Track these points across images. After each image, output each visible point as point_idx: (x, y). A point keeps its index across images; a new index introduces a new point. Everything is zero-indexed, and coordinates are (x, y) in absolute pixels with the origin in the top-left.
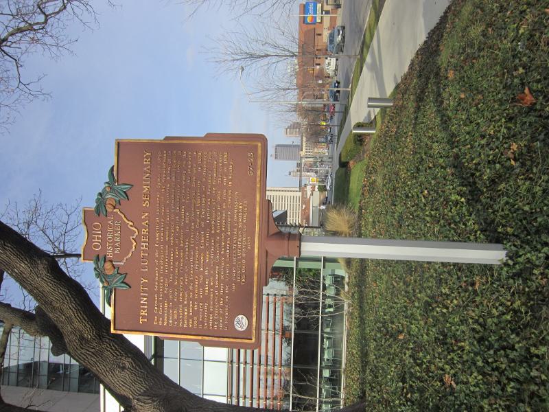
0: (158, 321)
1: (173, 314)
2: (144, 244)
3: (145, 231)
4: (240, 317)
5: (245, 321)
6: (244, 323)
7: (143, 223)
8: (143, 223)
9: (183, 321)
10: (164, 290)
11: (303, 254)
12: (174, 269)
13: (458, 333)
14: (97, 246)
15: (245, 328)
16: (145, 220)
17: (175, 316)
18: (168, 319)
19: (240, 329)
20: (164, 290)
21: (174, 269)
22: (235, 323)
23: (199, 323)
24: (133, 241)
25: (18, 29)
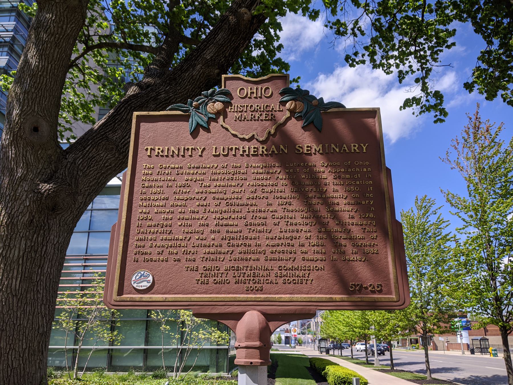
22: (142, 273)
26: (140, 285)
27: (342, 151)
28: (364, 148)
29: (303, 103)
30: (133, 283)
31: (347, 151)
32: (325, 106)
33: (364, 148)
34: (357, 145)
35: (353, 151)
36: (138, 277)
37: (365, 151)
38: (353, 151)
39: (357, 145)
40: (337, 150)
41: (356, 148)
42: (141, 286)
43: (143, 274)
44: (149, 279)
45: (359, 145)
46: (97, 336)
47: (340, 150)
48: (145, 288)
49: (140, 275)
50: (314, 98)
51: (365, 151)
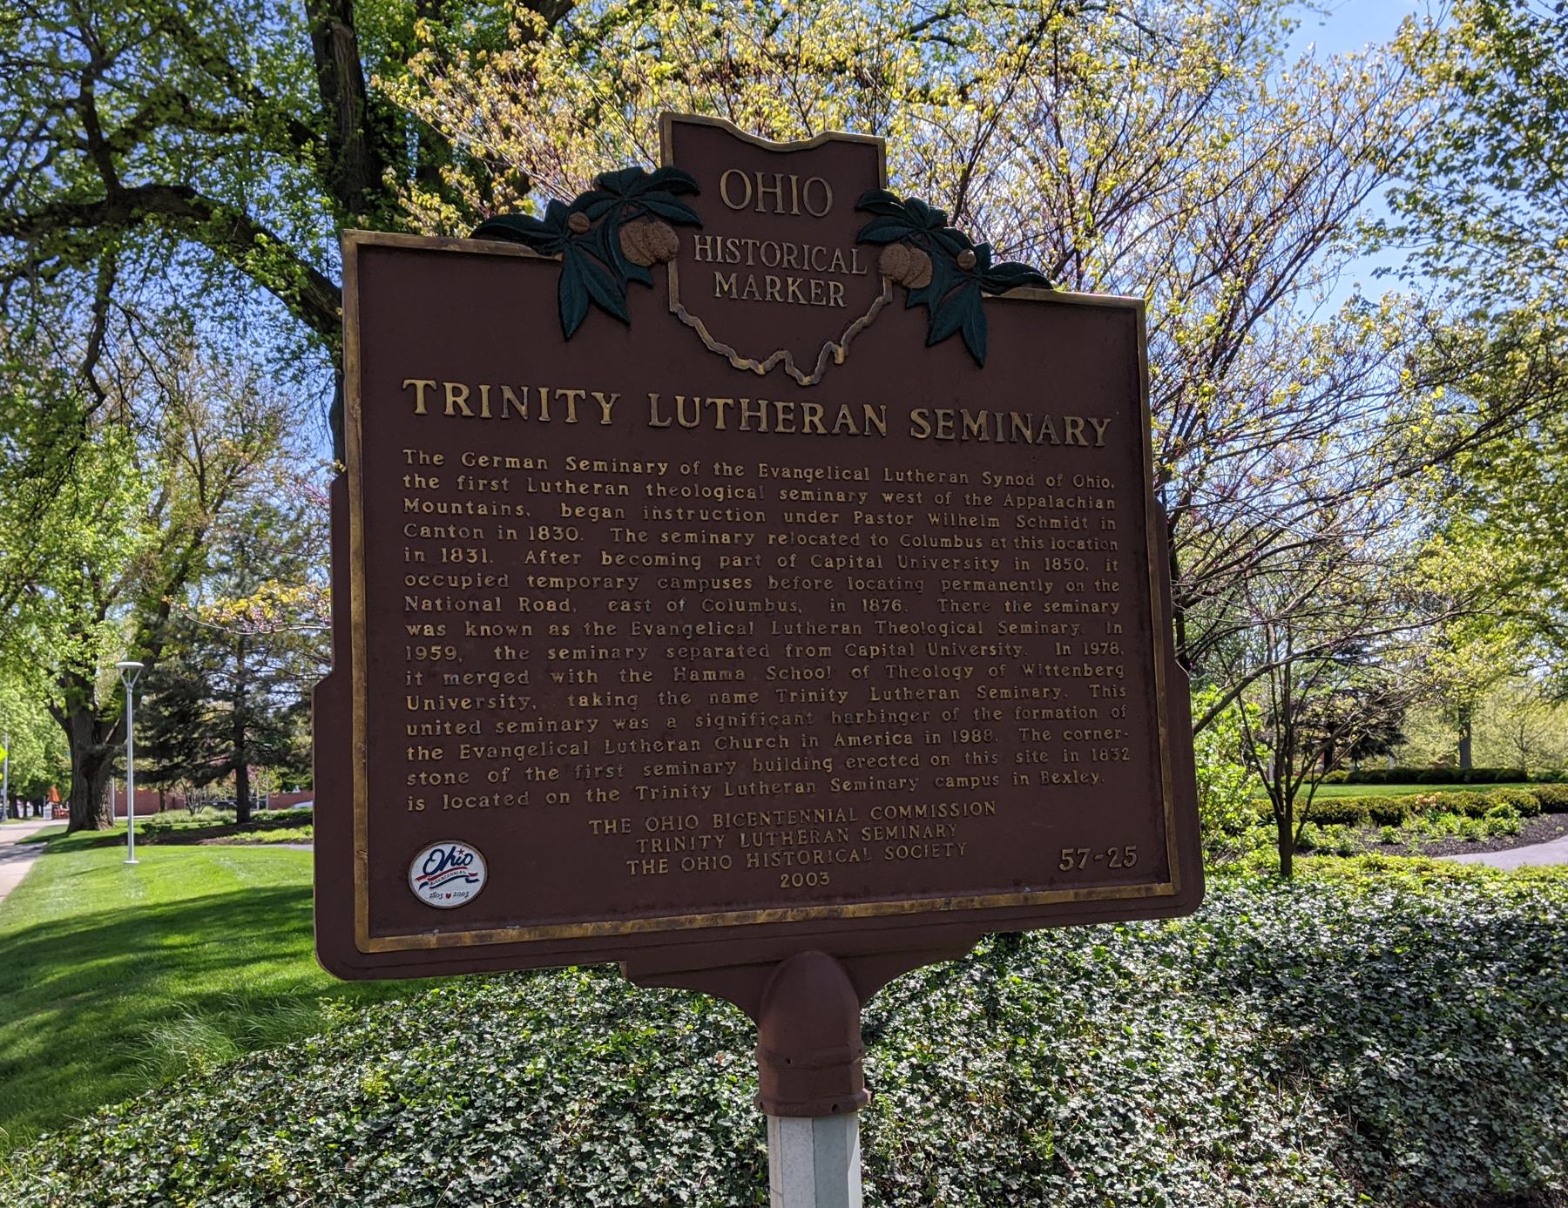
0: (427, 470)
1: (463, 545)
2: (763, 414)
3: (814, 418)
4: (477, 866)
5: (456, 892)
6: (442, 890)
7: (845, 410)
8: (845, 410)
9: (431, 593)
10: (573, 500)
11: (956, 338)
12: (669, 549)
13: (44, 1136)
14: (736, 184)
15: (425, 894)
16: (859, 416)
17: (456, 555)
18: (434, 519)
19: (416, 871)
20: (573, 500)
21: (669, 549)
22: (447, 849)
23: (432, 671)
24: (768, 363)
25: (1198, 578)
26: (439, 891)
27: (836, 430)
28: (606, 408)
29: (930, 255)
30: (416, 885)
31: (853, 429)
32: (996, 278)
33: (606, 408)
34: (818, 407)
35: (1069, 440)
36: (431, 867)
37: (606, 419)
38: (450, 410)
39: (818, 407)
40: (1028, 434)
41: (460, 400)
42: (448, 896)
43: (451, 856)
44: (471, 869)
45: (1087, 422)
46: (562, 1117)
47: (1035, 435)
48: (462, 900)
49: (438, 857)
50: (965, 242)
51: (606, 419)
